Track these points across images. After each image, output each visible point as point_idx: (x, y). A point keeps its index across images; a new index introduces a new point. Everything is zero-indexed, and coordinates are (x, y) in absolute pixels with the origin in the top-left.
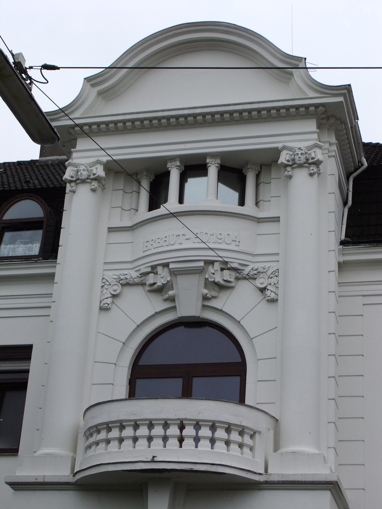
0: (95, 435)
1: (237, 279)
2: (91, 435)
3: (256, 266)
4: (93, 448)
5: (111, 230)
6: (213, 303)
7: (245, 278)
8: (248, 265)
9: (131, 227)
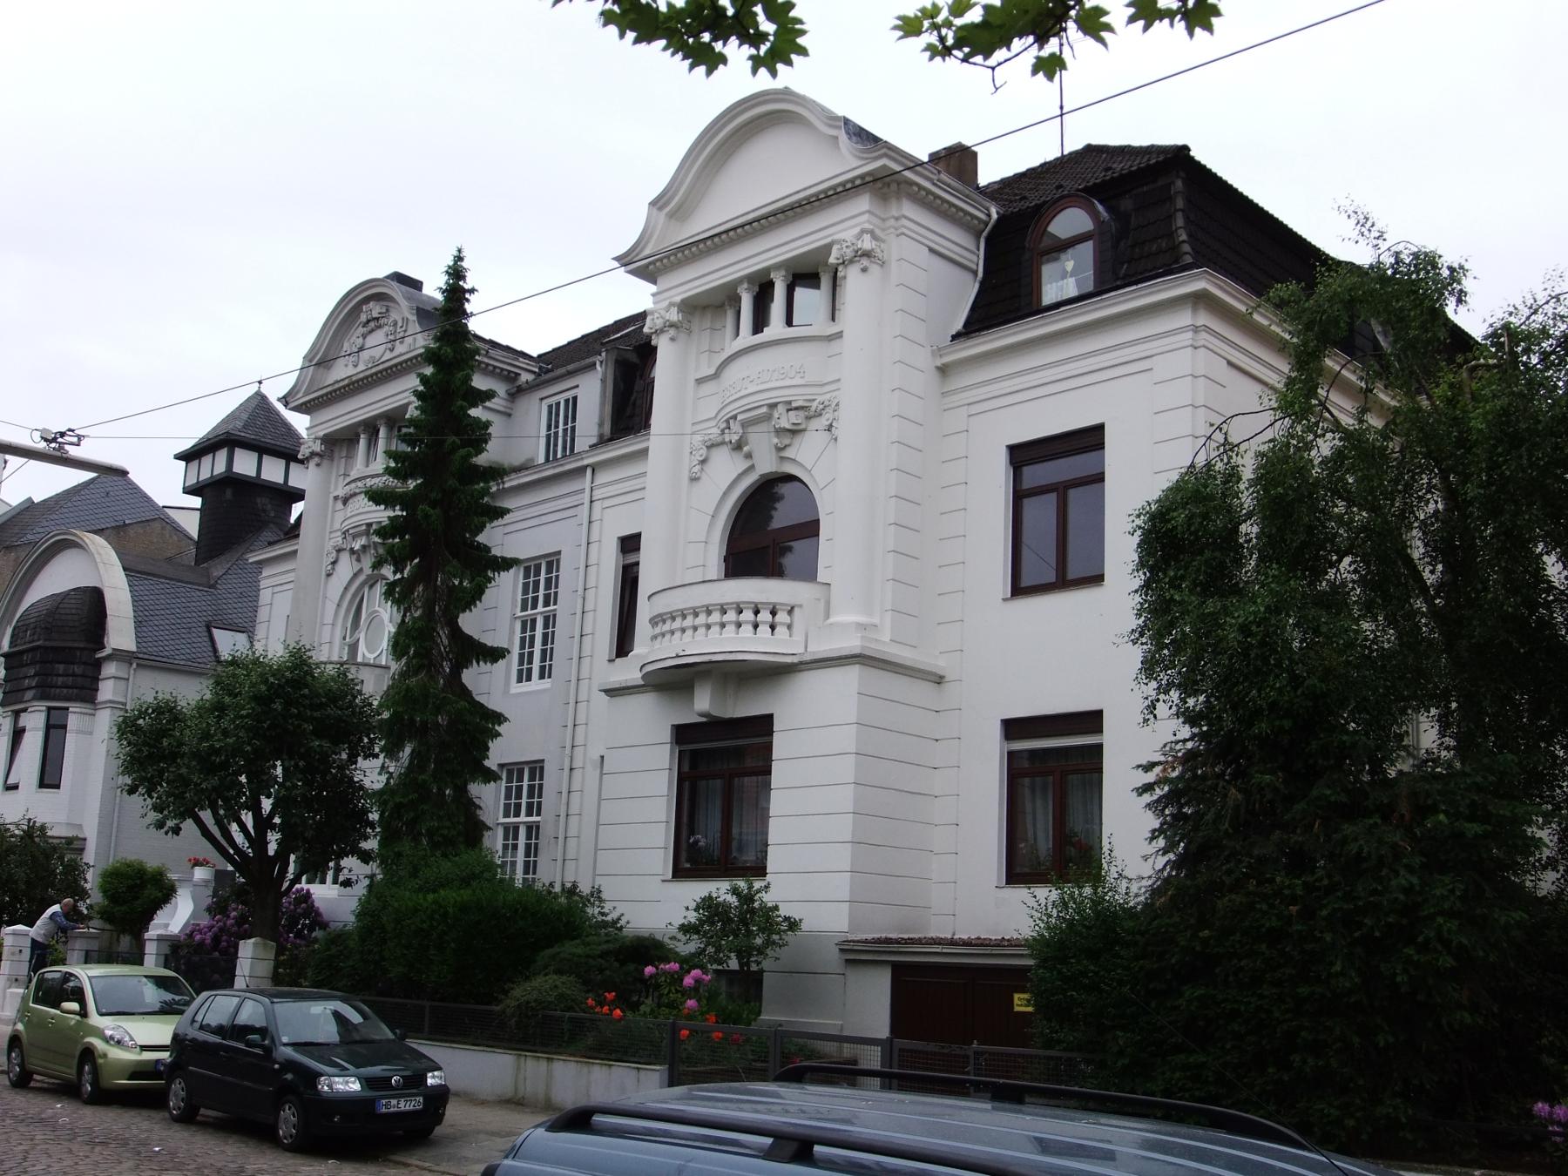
0: (668, 622)
1: (808, 418)
2: (657, 624)
3: (820, 399)
4: (659, 638)
5: (700, 381)
6: (786, 454)
7: (815, 416)
8: (814, 400)
9: (715, 374)
